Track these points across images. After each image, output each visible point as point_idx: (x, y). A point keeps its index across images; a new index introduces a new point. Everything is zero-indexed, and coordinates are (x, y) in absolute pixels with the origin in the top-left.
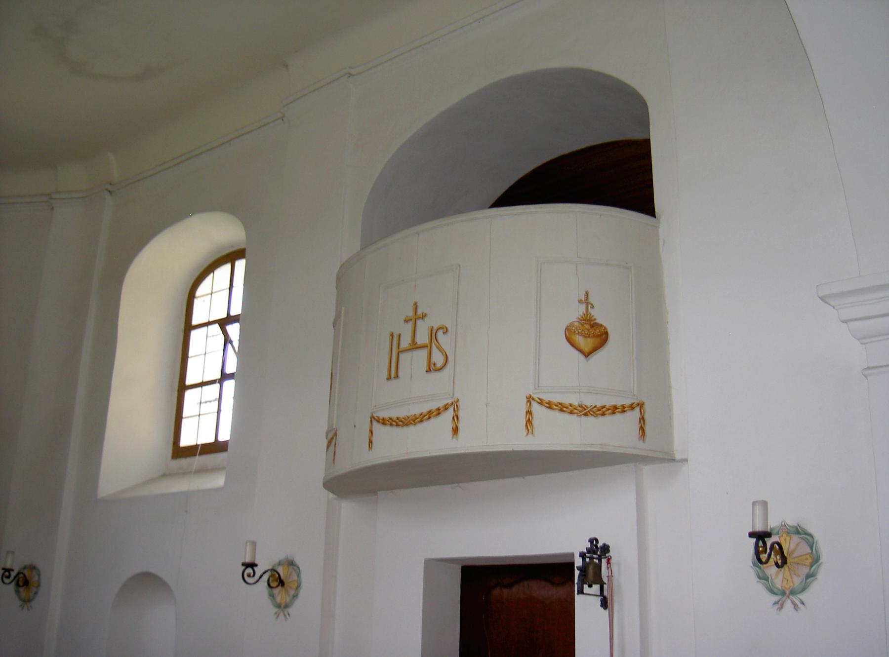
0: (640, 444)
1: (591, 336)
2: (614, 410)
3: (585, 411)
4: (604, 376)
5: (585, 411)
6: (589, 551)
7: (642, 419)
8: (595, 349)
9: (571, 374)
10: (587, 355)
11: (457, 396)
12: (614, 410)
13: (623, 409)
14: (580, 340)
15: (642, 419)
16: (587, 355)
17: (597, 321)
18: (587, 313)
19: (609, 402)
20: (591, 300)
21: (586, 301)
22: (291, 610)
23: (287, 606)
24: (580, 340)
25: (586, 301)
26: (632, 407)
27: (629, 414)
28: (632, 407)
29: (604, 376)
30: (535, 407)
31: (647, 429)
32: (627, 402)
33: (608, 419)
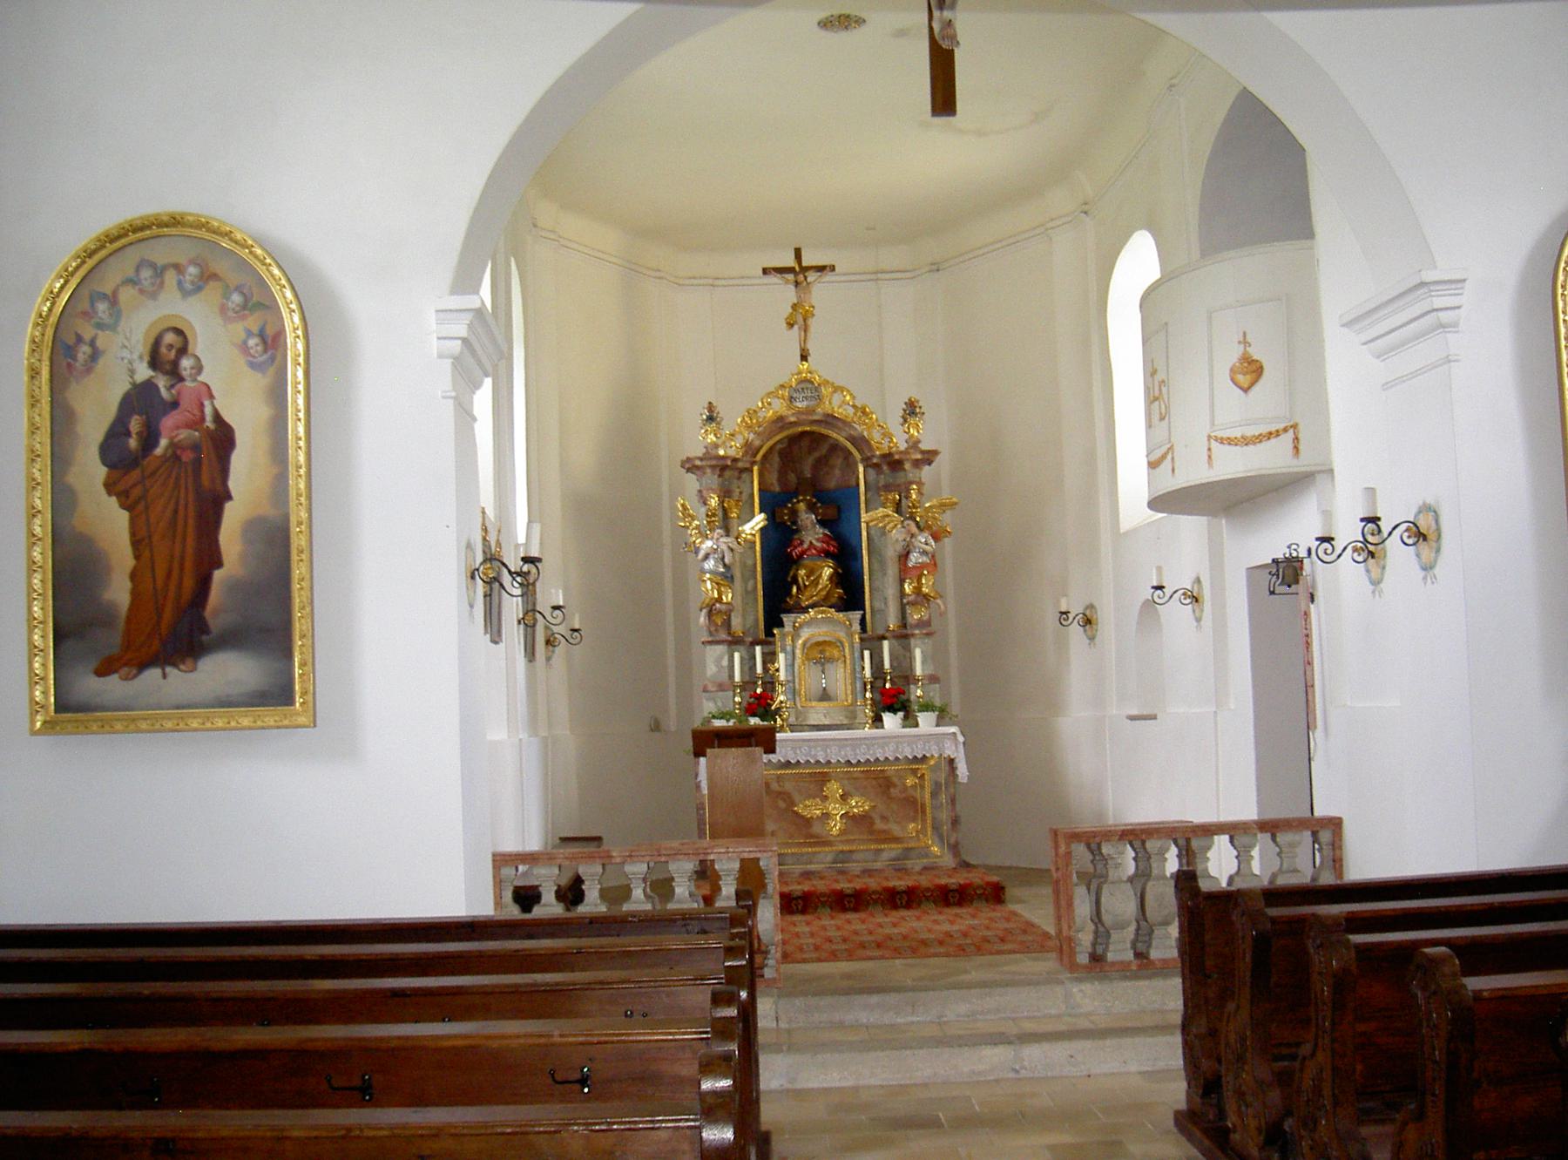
0: (1295, 462)
1: (1250, 371)
2: (1270, 435)
3: (1246, 441)
4: (1265, 404)
5: (1246, 441)
6: (525, 614)
7: (1296, 439)
8: (1253, 384)
9: (1238, 410)
10: (1246, 390)
11: (1297, 420)
12: (1270, 435)
13: (1278, 433)
14: (1240, 378)
15: (1296, 439)
16: (1246, 390)
17: (115, 677)
18: (1245, 353)
19: (1264, 429)
20: (1249, 338)
21: (1245, 342)
22: (1437, 571)
23: (1431, 568)
24: (1240, 378)
25: (1245, 342)
26: (1285, 430)
27: (1283, 436)
28: (1285, 430)
29: (1265, 404)
30: (1291, 433)
31: (1301, 447)
32: (1281, 426)
33: (1266, 445)
